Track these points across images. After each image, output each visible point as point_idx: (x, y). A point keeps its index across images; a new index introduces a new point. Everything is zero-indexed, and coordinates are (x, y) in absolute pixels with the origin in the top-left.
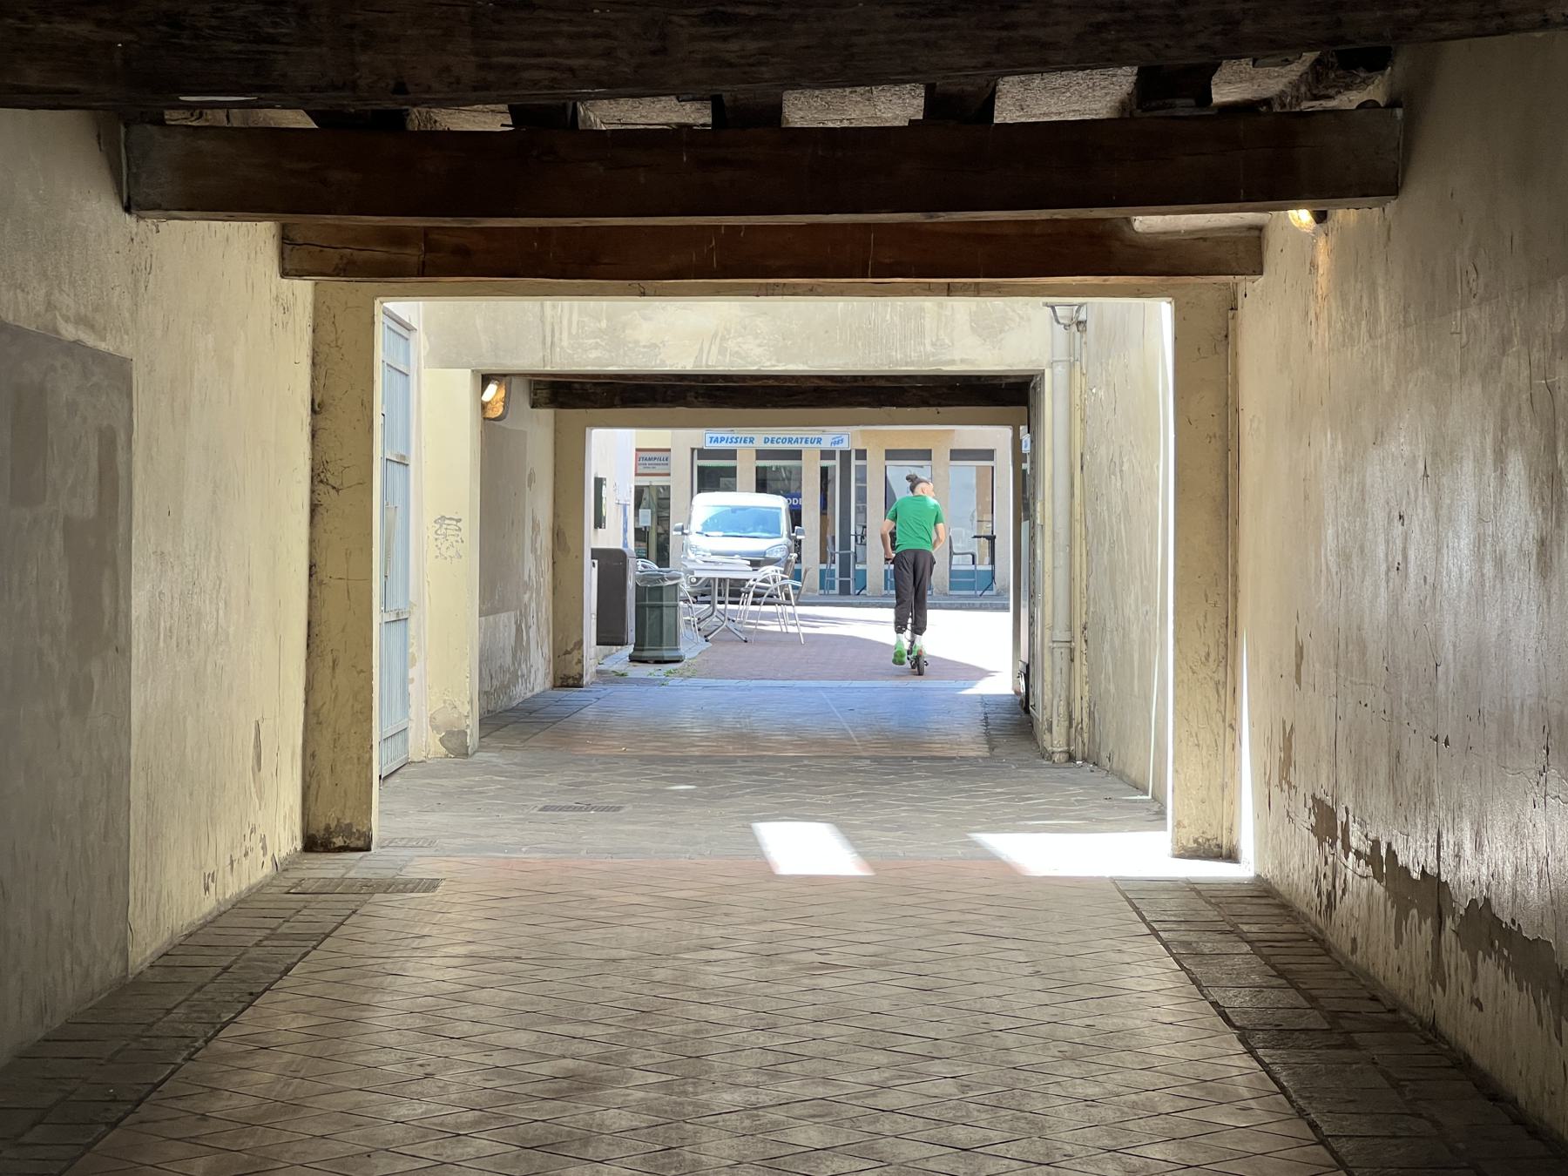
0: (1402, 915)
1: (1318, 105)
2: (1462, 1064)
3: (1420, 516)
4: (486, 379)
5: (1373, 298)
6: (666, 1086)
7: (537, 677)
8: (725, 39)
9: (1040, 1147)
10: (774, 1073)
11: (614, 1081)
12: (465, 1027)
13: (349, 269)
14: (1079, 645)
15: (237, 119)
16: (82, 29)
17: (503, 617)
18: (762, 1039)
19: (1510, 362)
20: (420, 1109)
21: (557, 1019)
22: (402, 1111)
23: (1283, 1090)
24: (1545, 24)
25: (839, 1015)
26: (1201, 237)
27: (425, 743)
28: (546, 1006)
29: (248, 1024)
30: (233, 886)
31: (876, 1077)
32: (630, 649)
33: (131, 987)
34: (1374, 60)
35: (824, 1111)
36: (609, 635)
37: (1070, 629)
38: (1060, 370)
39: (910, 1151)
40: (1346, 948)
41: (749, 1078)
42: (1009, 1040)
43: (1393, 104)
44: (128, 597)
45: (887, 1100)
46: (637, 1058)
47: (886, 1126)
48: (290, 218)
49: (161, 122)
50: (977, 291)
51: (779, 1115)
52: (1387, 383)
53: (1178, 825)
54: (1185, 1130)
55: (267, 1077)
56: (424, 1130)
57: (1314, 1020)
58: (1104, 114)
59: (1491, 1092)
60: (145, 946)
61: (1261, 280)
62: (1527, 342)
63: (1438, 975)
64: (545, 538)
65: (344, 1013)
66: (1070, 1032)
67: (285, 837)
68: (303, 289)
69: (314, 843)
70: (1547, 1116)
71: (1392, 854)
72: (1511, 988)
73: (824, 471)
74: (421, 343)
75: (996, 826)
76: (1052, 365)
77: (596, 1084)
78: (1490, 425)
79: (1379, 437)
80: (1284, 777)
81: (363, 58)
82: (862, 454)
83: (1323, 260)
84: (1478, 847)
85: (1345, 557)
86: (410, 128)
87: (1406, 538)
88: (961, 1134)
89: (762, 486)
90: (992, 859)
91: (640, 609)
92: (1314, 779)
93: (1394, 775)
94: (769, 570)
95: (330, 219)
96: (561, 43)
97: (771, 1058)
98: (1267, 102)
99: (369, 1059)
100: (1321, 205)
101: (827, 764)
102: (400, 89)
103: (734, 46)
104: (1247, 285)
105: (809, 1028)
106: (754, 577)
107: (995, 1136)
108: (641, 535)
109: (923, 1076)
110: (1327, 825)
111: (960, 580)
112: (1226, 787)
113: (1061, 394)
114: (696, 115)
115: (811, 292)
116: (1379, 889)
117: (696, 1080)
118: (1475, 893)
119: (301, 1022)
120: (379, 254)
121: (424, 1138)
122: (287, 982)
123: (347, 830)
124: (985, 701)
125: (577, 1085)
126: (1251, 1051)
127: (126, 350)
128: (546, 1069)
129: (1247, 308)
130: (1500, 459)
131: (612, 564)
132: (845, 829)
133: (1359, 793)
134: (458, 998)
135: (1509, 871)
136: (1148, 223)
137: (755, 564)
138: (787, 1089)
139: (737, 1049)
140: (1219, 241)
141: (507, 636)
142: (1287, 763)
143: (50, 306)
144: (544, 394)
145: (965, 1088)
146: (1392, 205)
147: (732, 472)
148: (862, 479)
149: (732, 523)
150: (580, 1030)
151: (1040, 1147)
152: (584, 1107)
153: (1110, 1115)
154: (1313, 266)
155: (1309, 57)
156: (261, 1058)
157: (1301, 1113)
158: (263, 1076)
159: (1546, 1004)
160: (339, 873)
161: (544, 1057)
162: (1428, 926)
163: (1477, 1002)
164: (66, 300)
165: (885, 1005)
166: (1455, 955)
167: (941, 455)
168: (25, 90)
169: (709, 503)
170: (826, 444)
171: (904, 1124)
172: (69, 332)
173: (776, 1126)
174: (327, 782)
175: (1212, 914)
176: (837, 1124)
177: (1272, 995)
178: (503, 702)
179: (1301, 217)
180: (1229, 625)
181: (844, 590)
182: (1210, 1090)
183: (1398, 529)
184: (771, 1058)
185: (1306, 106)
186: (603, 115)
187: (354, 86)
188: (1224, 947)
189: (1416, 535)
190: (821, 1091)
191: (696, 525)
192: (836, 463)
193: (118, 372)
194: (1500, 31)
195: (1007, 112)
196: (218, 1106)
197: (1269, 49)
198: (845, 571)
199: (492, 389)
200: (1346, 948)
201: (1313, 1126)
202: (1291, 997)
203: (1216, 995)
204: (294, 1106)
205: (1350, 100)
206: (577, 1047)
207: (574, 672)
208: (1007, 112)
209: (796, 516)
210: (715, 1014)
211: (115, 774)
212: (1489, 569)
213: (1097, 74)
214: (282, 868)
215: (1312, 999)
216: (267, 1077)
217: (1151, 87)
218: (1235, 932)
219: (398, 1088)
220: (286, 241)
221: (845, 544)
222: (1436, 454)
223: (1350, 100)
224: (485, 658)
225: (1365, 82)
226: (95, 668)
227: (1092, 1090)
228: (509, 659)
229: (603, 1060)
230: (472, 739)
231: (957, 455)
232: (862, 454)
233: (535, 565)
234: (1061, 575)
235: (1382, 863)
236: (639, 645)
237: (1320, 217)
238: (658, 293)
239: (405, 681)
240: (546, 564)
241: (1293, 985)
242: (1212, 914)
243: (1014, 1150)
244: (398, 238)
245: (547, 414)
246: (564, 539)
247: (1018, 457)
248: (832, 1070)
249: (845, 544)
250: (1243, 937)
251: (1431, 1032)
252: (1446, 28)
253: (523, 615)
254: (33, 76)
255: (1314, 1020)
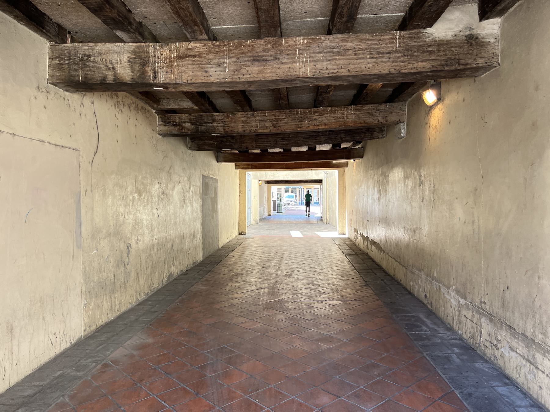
0: (364, 241)
1: (354, 148)
2: (370, 258)
3: (365, 195)
4: (259, 181)
5: (360, 170)
6: (279, 261)
7: (266, 215)
8: (284, 141)
9: (321, 267)
10: (291, 259)
11: (272, 260)
12: (256, 254)
13: (243, 168)
14: (328, 210)
15: (230, 152)
16: (211, 142)
17: (262, 208)
18: (290, 255)
19: (375, 177)
20: (251, 263)
21: (267, 253)
22: (249, 264)
23: (349, 261)
24: (378, 138)
25: (299, 253)
26: (341, 163)
27: (253, 222)
28: (265, 252)
29: (232, 254)
30: (230, 239)
31: (303, 260)
32: (277, 211)
33: (219, 250)
34: (360, 142)
35: (296, 263)
36: (274, 210)
37: (327, 208)
38: (325, 179)
39: (306, 268)
40: (358, 245)
41: (288, 260)
42: (318, 255)
43: (362, 147)
44: (217, 205)
45: (304, 262)
46: (275, 258)
47: (303, 265)
48: (236, 163)
49: (221, 152)
50: (315, 170)
51: (291, 264)
52: (362, 179)
53: (339, 231)
54: (338, 265)
55: (234, 260)
56: (251, 266)
57: (354, 253)
58: (329, 149)
59: (374, 261)
60: (221, 245)
61: (348, 168)
62: (377, 175)
63: (368, 248)
64: (267, 199)
65: (243, 253)
66: (325, 255)
67: (237, 233)
68: (238, 170)
69: (240, 234)
70: (380, 264)
71: (363, 234)
72: (375, 249)
73: (299, 191)
74: (252, 177)
75: (318, 231)
76: (324, 178)
77: (271, 260)
78: (373, 184)
79: (361, 186)
80: (351, 225)
81: (243, 145)
82: (303, 189)
83: (354, 166)
84: (372, 233)
85: (357, 200)
86: (292, 148)
87: (364, 197)
88: (312, 266)
89: (292, 192)
90: (317, 235)
91: (278, 207)
92: (354, 225)
93: (363, 225)
94: (292, 202)
95: (240, 163)
96: (265, 142)
97: (290, 258)
98: (348, 147)
99: (245, 258)
100: (354, 159)
101: (299, 224)
102: (247, 148)
103: (285, 142)
104: (346, 168)
105: (295, 254)
106: (291, 203)
107: (316, 266)
108: (278, 198)
109: (308, 259)
110: (356, 231)
111: (315, 203)
112: (344, 227)
113: (325, 181)
114: (282, 150)
115: (296, 170)
116: (361, 238)
117: (282, 260)
118: (372, 238)
119: (238, 254)
120: (246, 167)
121: (251, 266)
122: (236, 249)
123: (244, 232)
124: (317, 217)
125: (269, 261)
126: (346, 257)
127: (217, 178)
128: (265, 259)
129: (346, 171)
130: (374, 188)
131: (274, 202)
132: (301, 232)
133: (359, 227)
134: (255, 251)
135: (375, 236)
136: (335, 162)
137: (291, 201)
138: (292, 261)
139: (287, 257)
140: (343, 163)
141: (262, 210)
142: (351, 224)
143: (209, 173)
144: (266, 182)
145: (313, 261)
146: (362, 159)
147: (289, 191)
148: (303, 192)
149: (289, 197)
150: (269, 255)
151: (321, 267)
152: (269, 263)
153: (329, 264)
154: (354, 166)
155: (352, 142)
156: (233, 258)
157: (351, 264)
158: (233, 260)
159: (379, 251)
160: (242, 237)
161: (265, 257)
162: (367, 242)
163: (372, 251)
164: (211, 173)
165: (304, 252)
166: (370, 246)
167: (313, 189)
168: (205, 149)
169: (287, 194)
170: (299, 188)
171: (306, 265)
172: (211, 176)
173: (291, 265)
174: (241, 227)
175: (342, 241)
176: (298, 265)
177: (349, 250)
178: (262, 218)
179: (352, 160)
180: (344, 207)
181: (302, 204)
182: (341, 261)
183: (363, 197)
184: (290, 258)
185: (352, 148)
186: (271, 150)
187: (242, 148)
188: (343, 245)
189: (365, 197)
190: (296, 261)
191: (284, 197)
192: (300, 190)
193: (216, 180)
194: (373, 139)
195: (317, 149)
196: (229, 263)
197: (347, 141)
198: (302, 202)
199: (260, 181)
200: (358, 245)
201: (353, 265)
202: (351, 250)
203: (342, 250)
204: (237, 263)
205: (357, 147)
206: (269, 256)
207: (270, 214)
208: (317, 149)
209: (296, 196)
210: (285, 253)
211: (217, 226)
212: (373, 201)
213: (328, 145)
214: (236, 237)
215: (353, 251)
216: (234, 260)
217: (339, 145)
218: (345, 243)
219: (248, 261)
220: (236, 165)
221: (302, 199)
222: (367, 188)
223: (357, 147)
224: (260, 213)
225: (359, 145)
226: (215, 214)
227: (328, 261)
228: (262, 213)
229: (271, 258)
230: (258, 222)
231: (314, 189)
232: (303, 189)
233: (265, 202)
234: (325, 202)
235: (362, 235)
236: (278, 211)
237: (354, 161)
238: (278, 171)
239: (250, 215)
240: (267, 202)
241: (352, 249)
242: (342, 241)
243: (318, 268)
244: (248, 165)
245: (267, 184)
246: (269, 199)
247: (321, 189)
248: (298, 259)
249: (302, 199)
250: (346, 244)
251: (367, 254)
252: (367, 139)
253: (264, 207)
254: (206, 147)
255: (354, 253)
